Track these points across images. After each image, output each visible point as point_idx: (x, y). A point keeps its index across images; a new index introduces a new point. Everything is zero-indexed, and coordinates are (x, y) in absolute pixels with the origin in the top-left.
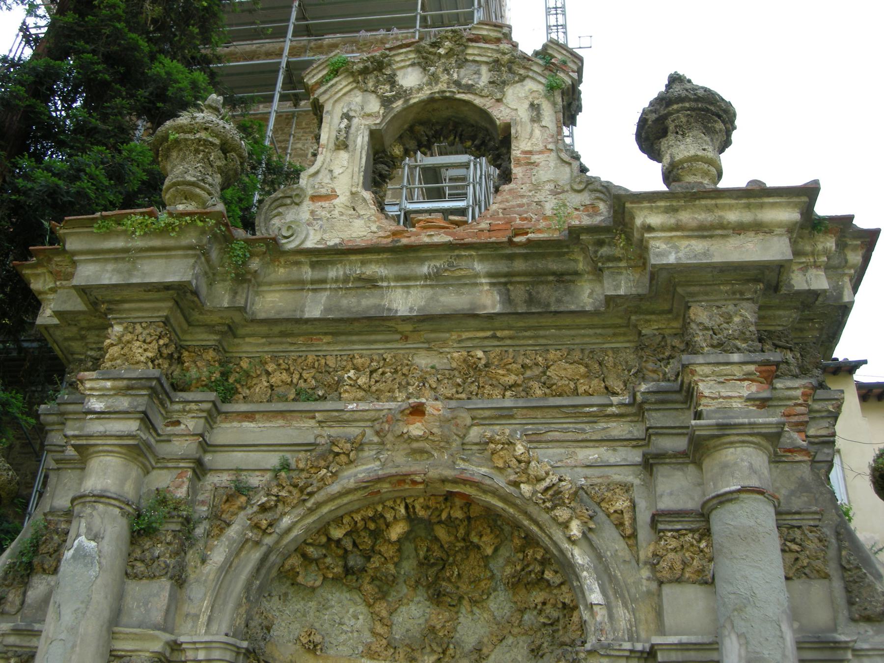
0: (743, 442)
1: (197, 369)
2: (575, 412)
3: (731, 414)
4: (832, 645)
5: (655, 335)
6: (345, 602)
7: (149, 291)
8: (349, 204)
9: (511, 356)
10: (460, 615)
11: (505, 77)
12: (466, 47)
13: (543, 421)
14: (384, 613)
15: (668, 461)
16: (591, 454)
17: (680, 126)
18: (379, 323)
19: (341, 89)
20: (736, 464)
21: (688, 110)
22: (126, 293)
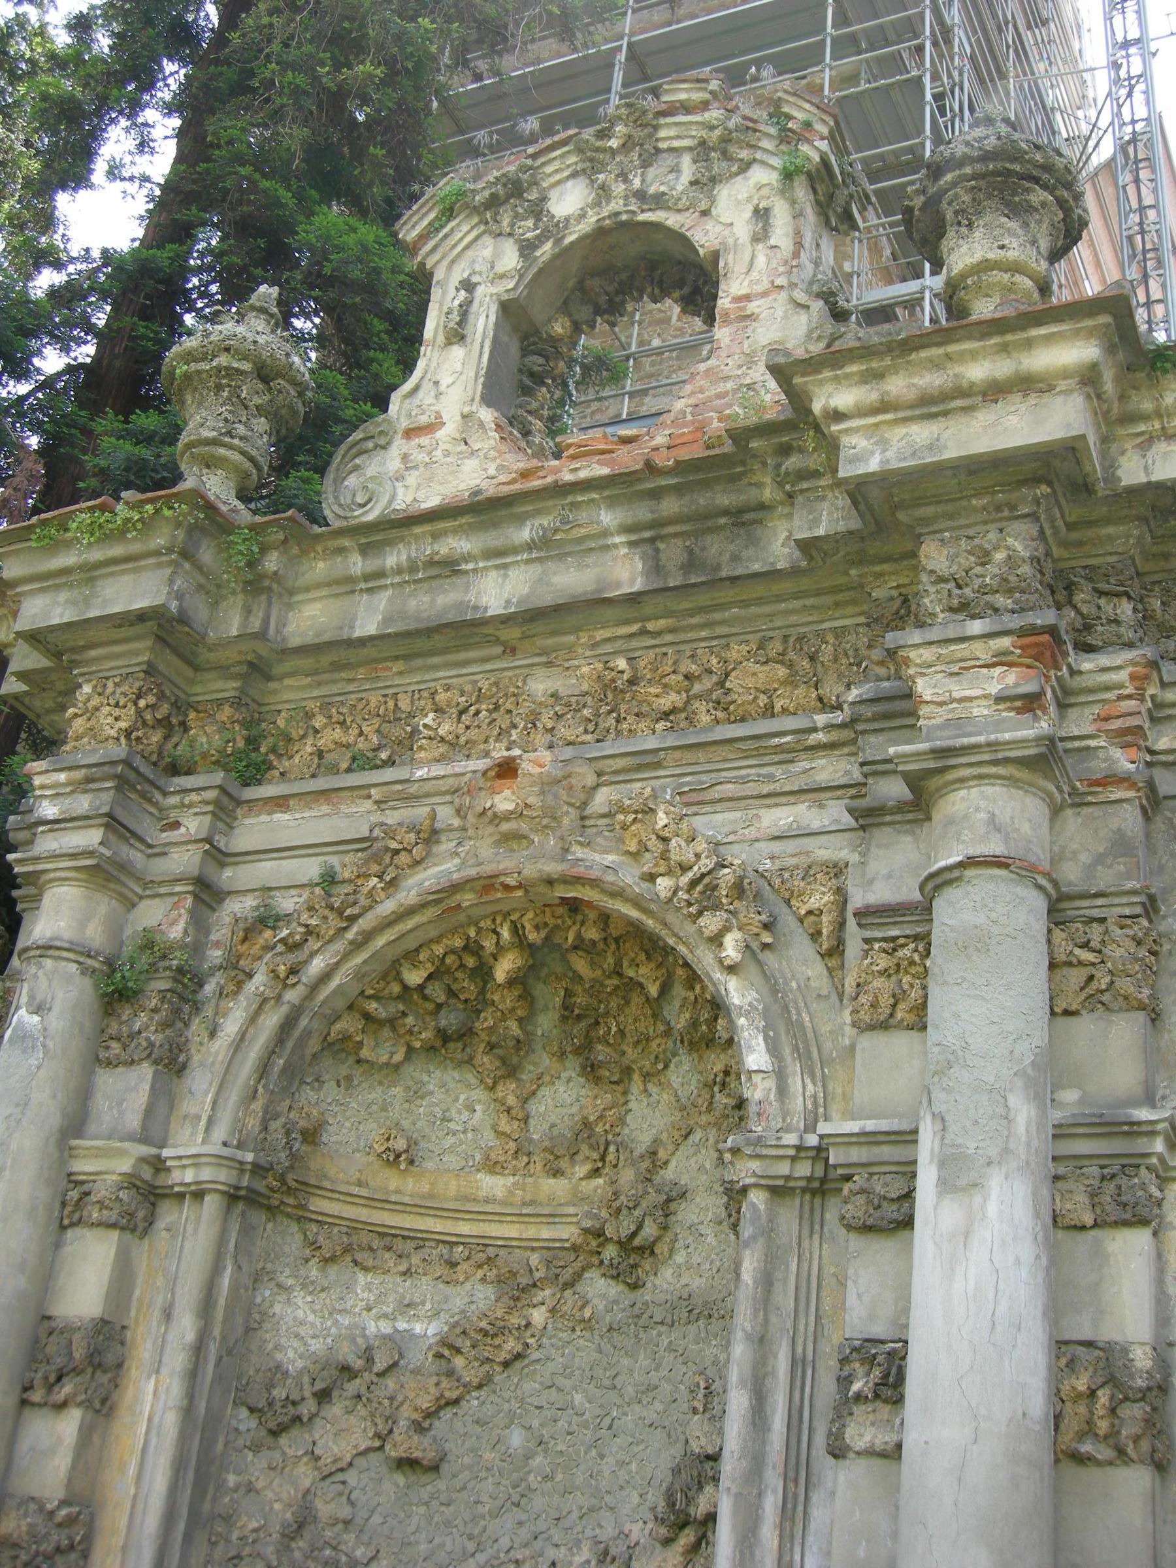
0: (981, 777)
1: (205, 737)
2: (758, 748)
3: (970, 729)
4: (1126, 1128)
5: (892, 599)
6: (451, 1085)
7: (120, 626)
8: (458, 436)
9: (670, 662)
10: (630, 1097)
11: (715, 171)
12: (656, 128)
13: (707, 767)
14: (511, 1101)
15: (888, 818)
16: (781, 817)
17: (963, 211)
18: (466, 633)
19: (462, 239)
20: (966, 817)
21: (973, 179)
22: (93, 634)
